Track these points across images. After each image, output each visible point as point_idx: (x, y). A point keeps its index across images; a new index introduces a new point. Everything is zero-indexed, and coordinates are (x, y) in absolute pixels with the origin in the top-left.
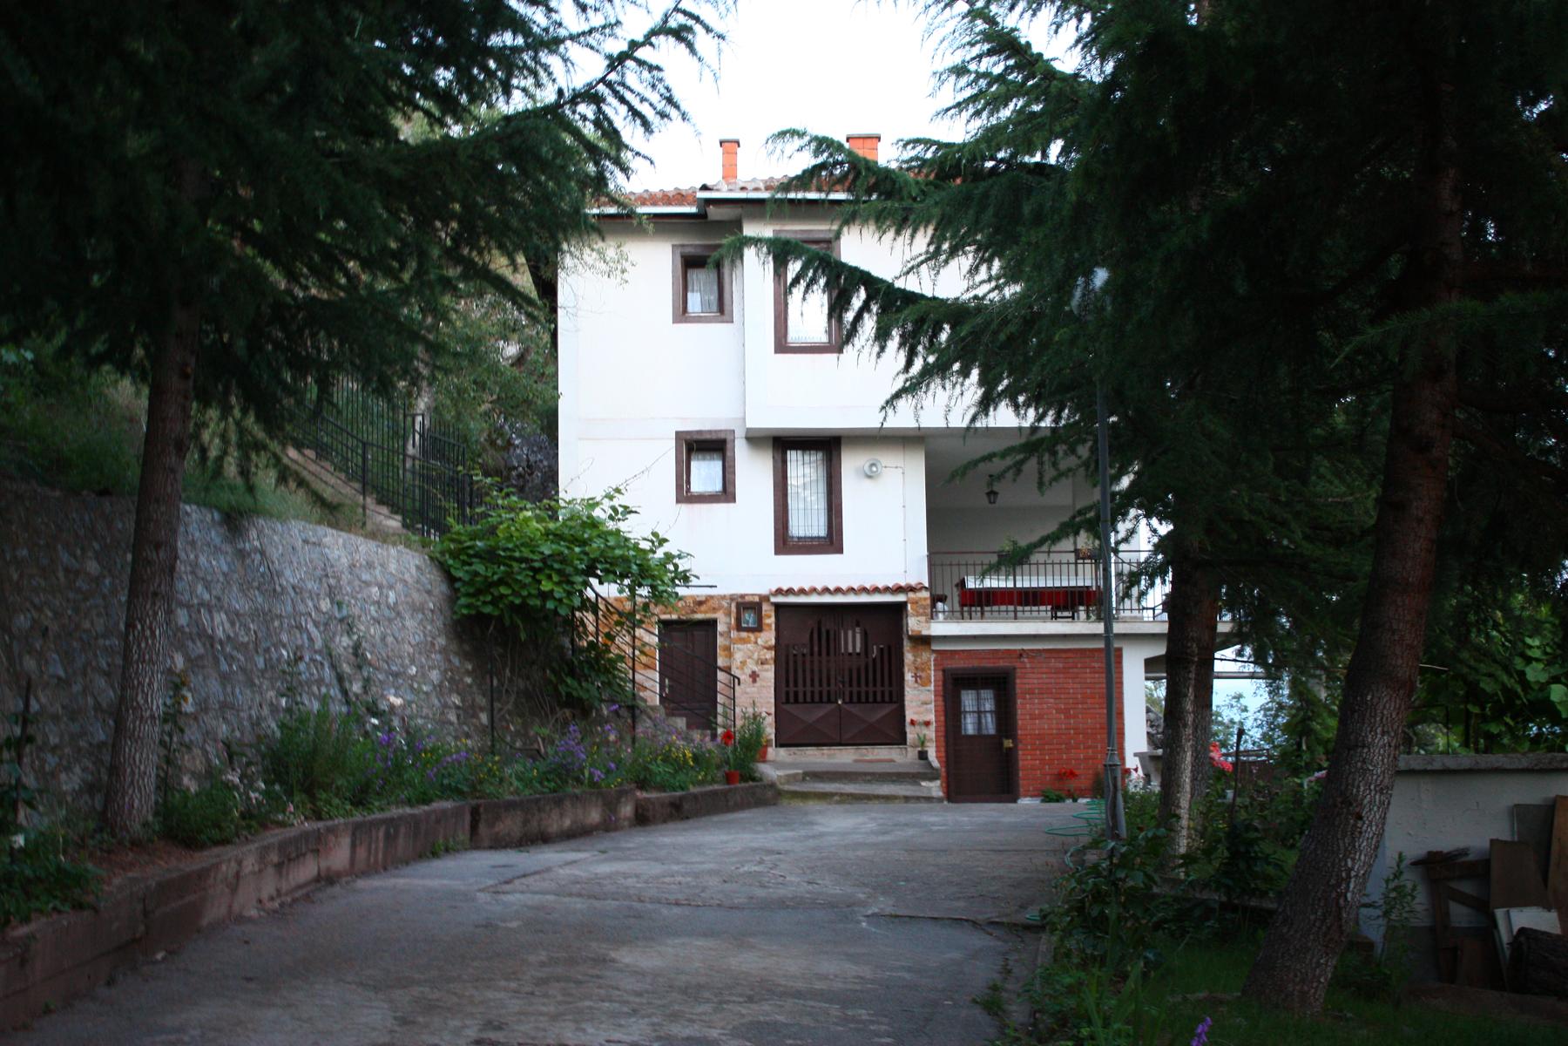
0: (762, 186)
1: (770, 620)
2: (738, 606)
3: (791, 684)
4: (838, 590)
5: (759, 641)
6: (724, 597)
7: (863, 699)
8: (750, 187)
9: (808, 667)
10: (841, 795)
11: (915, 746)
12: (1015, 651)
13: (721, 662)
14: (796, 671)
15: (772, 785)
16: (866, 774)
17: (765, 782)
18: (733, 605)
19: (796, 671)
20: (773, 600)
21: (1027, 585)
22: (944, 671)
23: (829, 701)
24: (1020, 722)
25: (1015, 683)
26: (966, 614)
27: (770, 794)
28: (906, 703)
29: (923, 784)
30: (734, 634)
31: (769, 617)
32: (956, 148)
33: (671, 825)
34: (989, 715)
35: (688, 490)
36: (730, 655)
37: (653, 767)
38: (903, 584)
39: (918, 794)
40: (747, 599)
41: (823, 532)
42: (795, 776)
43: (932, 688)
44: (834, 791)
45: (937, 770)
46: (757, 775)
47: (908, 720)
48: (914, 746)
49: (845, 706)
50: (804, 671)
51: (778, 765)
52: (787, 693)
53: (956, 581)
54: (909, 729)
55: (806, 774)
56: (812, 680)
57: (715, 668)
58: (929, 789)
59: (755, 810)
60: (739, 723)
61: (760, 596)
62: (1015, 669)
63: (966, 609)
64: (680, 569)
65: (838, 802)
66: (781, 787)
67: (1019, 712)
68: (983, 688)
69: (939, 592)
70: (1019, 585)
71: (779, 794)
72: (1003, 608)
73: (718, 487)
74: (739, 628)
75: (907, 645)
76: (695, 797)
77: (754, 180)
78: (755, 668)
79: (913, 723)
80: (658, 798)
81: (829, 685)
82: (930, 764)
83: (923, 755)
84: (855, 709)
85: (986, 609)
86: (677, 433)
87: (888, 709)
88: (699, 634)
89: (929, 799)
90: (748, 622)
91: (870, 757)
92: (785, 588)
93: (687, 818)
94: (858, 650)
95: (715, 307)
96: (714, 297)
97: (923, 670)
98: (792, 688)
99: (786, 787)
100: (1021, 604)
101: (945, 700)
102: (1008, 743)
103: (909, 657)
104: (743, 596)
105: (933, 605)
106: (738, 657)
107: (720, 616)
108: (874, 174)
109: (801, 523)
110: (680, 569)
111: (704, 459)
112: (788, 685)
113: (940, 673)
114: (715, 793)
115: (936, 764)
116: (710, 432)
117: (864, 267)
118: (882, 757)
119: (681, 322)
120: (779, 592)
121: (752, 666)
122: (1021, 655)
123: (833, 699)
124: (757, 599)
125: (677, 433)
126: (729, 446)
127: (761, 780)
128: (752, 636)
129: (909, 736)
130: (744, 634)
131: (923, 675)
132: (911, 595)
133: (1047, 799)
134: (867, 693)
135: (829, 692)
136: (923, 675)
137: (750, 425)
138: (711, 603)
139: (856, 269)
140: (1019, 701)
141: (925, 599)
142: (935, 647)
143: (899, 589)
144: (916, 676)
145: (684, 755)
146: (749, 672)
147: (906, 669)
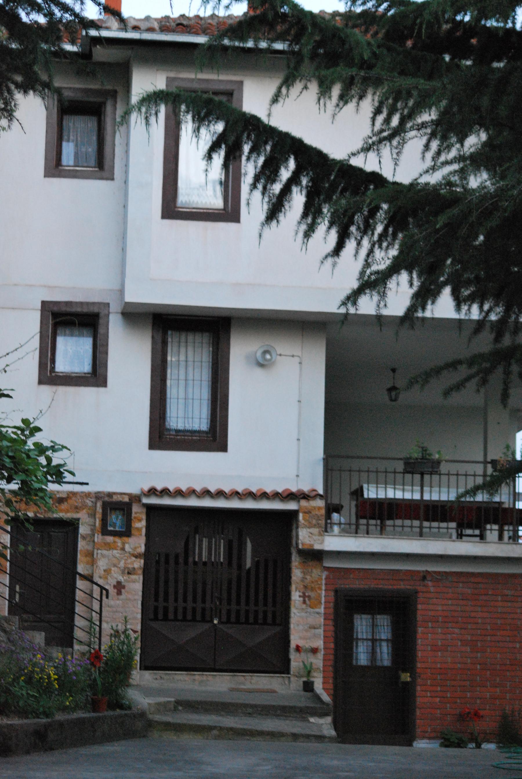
0: (156, 25)
1: (142, 524)
2: (105, 505)
3: (161, 598)
4: (220, 494)
5: (127, 547)
6: (88, 495)
7: (243, 619)
8: (143, 26)
9: (172, 577)
10: (221, 729)
11: (300, 676)
12: (418, 572)
13: (81, 568)
14: (166, 582)
15: (142, 715)
16: (246, 706)
17: (134, 710)
18: (99, 505)
19: (166, 582)
20: (145, 501)
21: (435, 497)
22: (336, 591)
23: (204, 620)
24: (419, 654)
25: (416, 610)
26: (363, 528)
27: (139, 724)
28: (292, 626)
29: (312, 720)
30: (98, 538)
31: (140, 520)
32: (411, 8)
33: (35, 757)
34: (384, 644)
35: (53, 368)
36: (93, 562)
37: (15, 689)
38: (294, 489)
39: (308, 732)
40: (115, 498)
41: (204, 426)
42: (165, 705)
43: (322, 610)
44: (211, 724)
45: (328, 705)
46: (125, 702)
47: (293, 645)
48: (298, 676)
49: (221, 626)
50: (176, 582)
51: (147, 692)
52: (156, 608)
53: (355, 486)
54: (293, 656)
55: (178, 703)
56: (166, 594)
57: (75, 573)
58: (320, 726)
59: (123, 742)
60: (106, 640)
61: (130, 495)
62: (417, 592)
63: (363, 521)
64: (55, 462)
65: (217, 738)
66: (150, 717)
67: (419, 641)
68: (379, 614)
69: (336, 501)
70: (426, 497)
71: (150, 725)
72: (408, 522)
73: (86, 367)
74: (105, 532)
75: (295, 560)
76: (61, 724)
77: (148, 18)
78: (121, 578)
79: (298, 649)
80: (22, 726)
81: (204, 601)
82: (318, 698)
83: (308, 687)
84: (231, 630)
85: (389, 522)
86: (43, 303)
87: (270, 632)
88: (57, 534)
89: (320, 738)
90: (114, 525)
91: (248, 686)
92: (159, 487)
93: (52, 749)
94: (204, 560)
95: (93, 161)
96: (91, 149)
97: (312, 589)
98: (161, 604)
99: (158, 717)
100: (427, 520)
101: (336, 626)
102: (406, 677)
103: (297, 574)
104: (110, 495)
105: (328, 516)
106: (102, 564)
107: (83, 516)
108: (321, 30)
109: (181, 414)
110: (55, 462)
111: (72, 335)
112: (156, 600)
113: (332, 594)
114: (81, 721)
115: (326, 698)
116: (81, 304)
117: (296, 133)
118: (260, 686)
119: (53, 176)
120: (153, 492)
121: (117, 576)
122: (424, 578)
123: (208, 618)
124: (126, 499)
125: (43, 303)
126: (101, 321)
127: (129, 708)
128: (119, 541)
129: (294, 665)
130: (110, 539)
131: (312, 594)
132: (304, 503)
133: (447, 743)
134: (265, 613)
135: (204, 610)
136: (312, 594)
137: (129, 298)
138: (72, 501)
139: (287, 135)
140: (420, 630)
141: (319, 508)
142: (328, 564)
143: (290, 496)
144: (304, 596)
145: (49, 677)
146: (114, 582)
147: (293, 587)
